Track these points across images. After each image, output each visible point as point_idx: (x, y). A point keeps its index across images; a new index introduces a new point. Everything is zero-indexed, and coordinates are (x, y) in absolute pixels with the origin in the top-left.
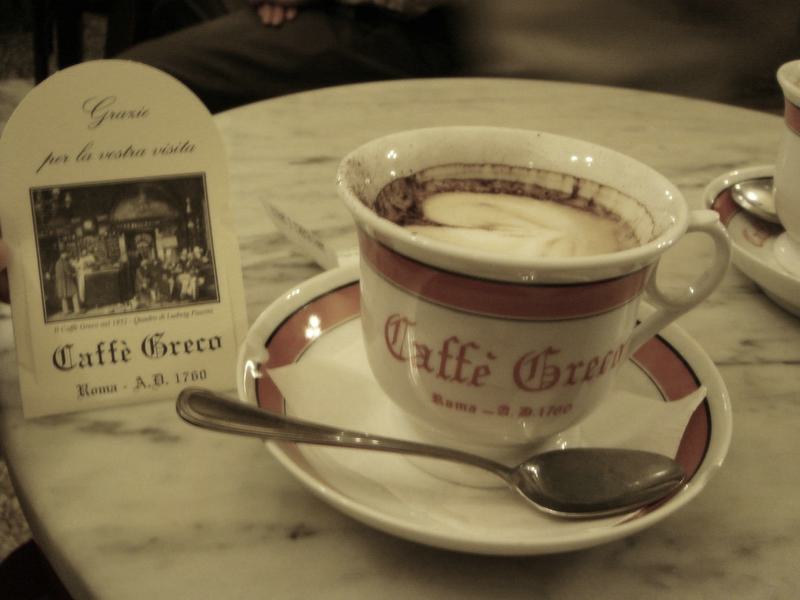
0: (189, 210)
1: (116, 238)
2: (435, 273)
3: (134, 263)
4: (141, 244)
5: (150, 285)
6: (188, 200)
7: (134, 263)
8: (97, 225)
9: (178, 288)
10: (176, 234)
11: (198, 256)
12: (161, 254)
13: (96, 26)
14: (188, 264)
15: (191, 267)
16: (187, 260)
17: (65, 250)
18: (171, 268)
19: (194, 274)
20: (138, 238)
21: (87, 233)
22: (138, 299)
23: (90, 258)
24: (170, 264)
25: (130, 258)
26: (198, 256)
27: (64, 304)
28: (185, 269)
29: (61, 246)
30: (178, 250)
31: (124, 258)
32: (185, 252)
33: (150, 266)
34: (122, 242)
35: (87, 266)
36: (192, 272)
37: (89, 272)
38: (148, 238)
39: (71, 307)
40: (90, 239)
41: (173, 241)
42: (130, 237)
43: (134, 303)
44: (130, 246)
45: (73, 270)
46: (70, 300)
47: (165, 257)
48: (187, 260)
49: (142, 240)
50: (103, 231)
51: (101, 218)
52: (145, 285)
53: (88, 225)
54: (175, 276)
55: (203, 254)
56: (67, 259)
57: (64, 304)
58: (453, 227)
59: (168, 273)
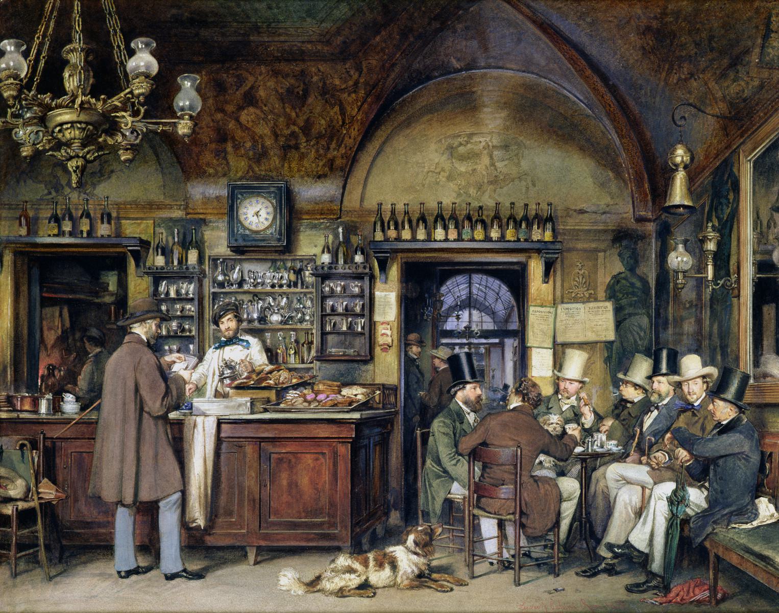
0: (679, 194)
1: (367, 277)
2: (487, 510)
3: (418, 405)
4: (468, 305)
5: (480, 492)
6: (680, 155)
7: (418, 405)
8: (290, 214)
9: (590, 521)
10: (612, 294)
11: (696, 392)
12: (541, 365)
13: (405, 537)
14: (648, 421)
15: (659, 434)
16: (647, 406)
17: (155, 309)
18: (573, 430)
19: (671, 470)
20: (454, 290)
21: (246, 247)
22: (426, 546)
23: (252, 353)
24: (576, 417)
25: (409, 366)
26: (696, 392)
27: (124, 525)
28: (635, 445)
29: (138, 287)
30: (616, 357)
31: (387, 368)
32: (641, 369)
33: (489, 409)
34: (388, 300)
35: (238, 381)
36: (661, 457)
37: (239, 406)
38: (497, 293)
39: (149, 546)
40: (261, 273)
41: (596, 320)
42: (424, 280)
43: (406, 558)
44: (417, 312)
45: (175, 395)
46: (148, 512)
47: (556, 383)
48: (647, 406)
49: (469, 303)
50: (312, 245)
51: (311, 192)
52: (458, 491)
53: (257, 215)
54: (590, 464)
55: (717, 390)
56: (155, 346)
57: (124, 525)
58: (632, 484)
59: (559, 448)
